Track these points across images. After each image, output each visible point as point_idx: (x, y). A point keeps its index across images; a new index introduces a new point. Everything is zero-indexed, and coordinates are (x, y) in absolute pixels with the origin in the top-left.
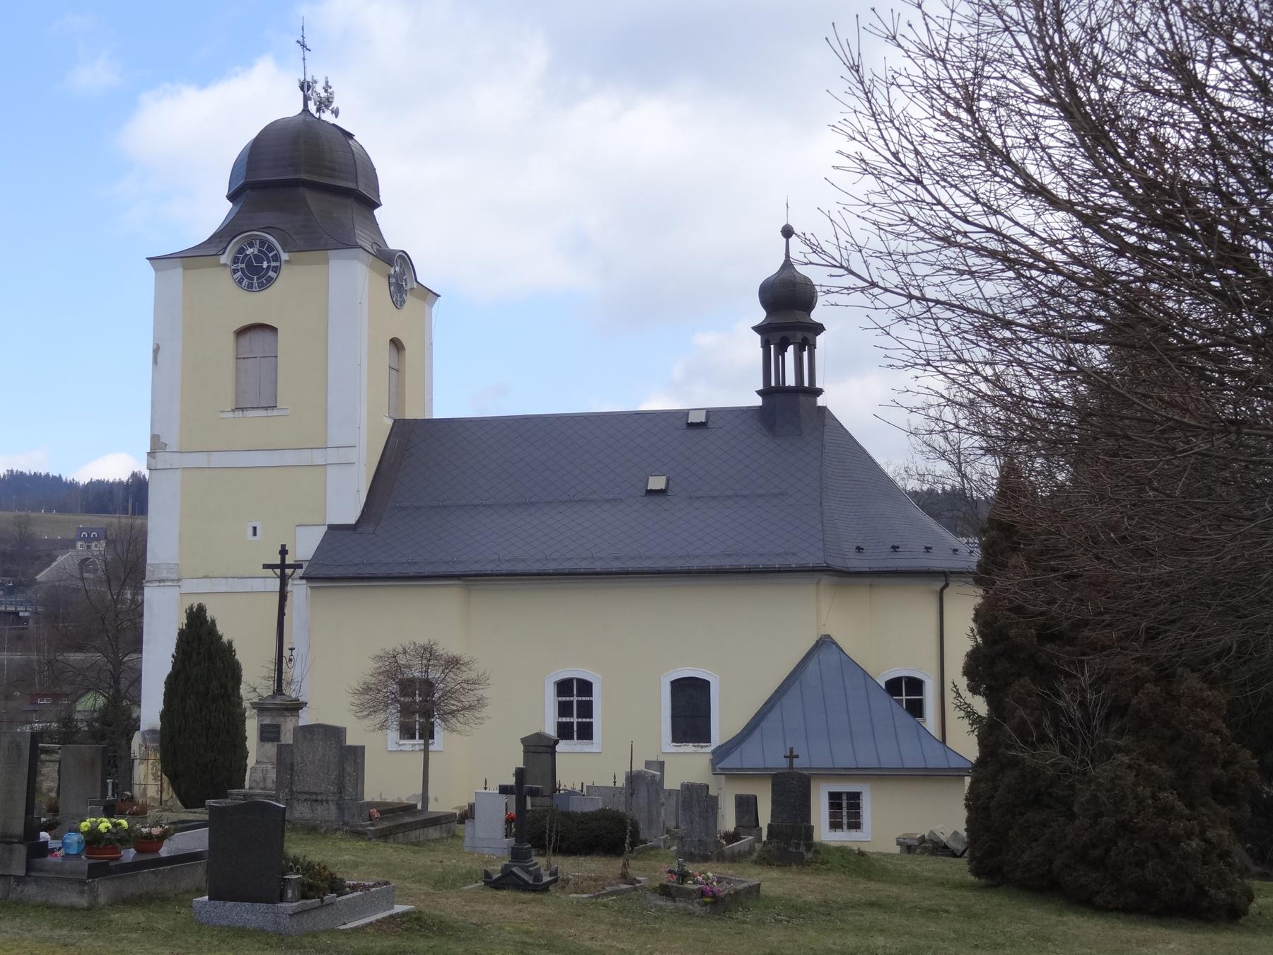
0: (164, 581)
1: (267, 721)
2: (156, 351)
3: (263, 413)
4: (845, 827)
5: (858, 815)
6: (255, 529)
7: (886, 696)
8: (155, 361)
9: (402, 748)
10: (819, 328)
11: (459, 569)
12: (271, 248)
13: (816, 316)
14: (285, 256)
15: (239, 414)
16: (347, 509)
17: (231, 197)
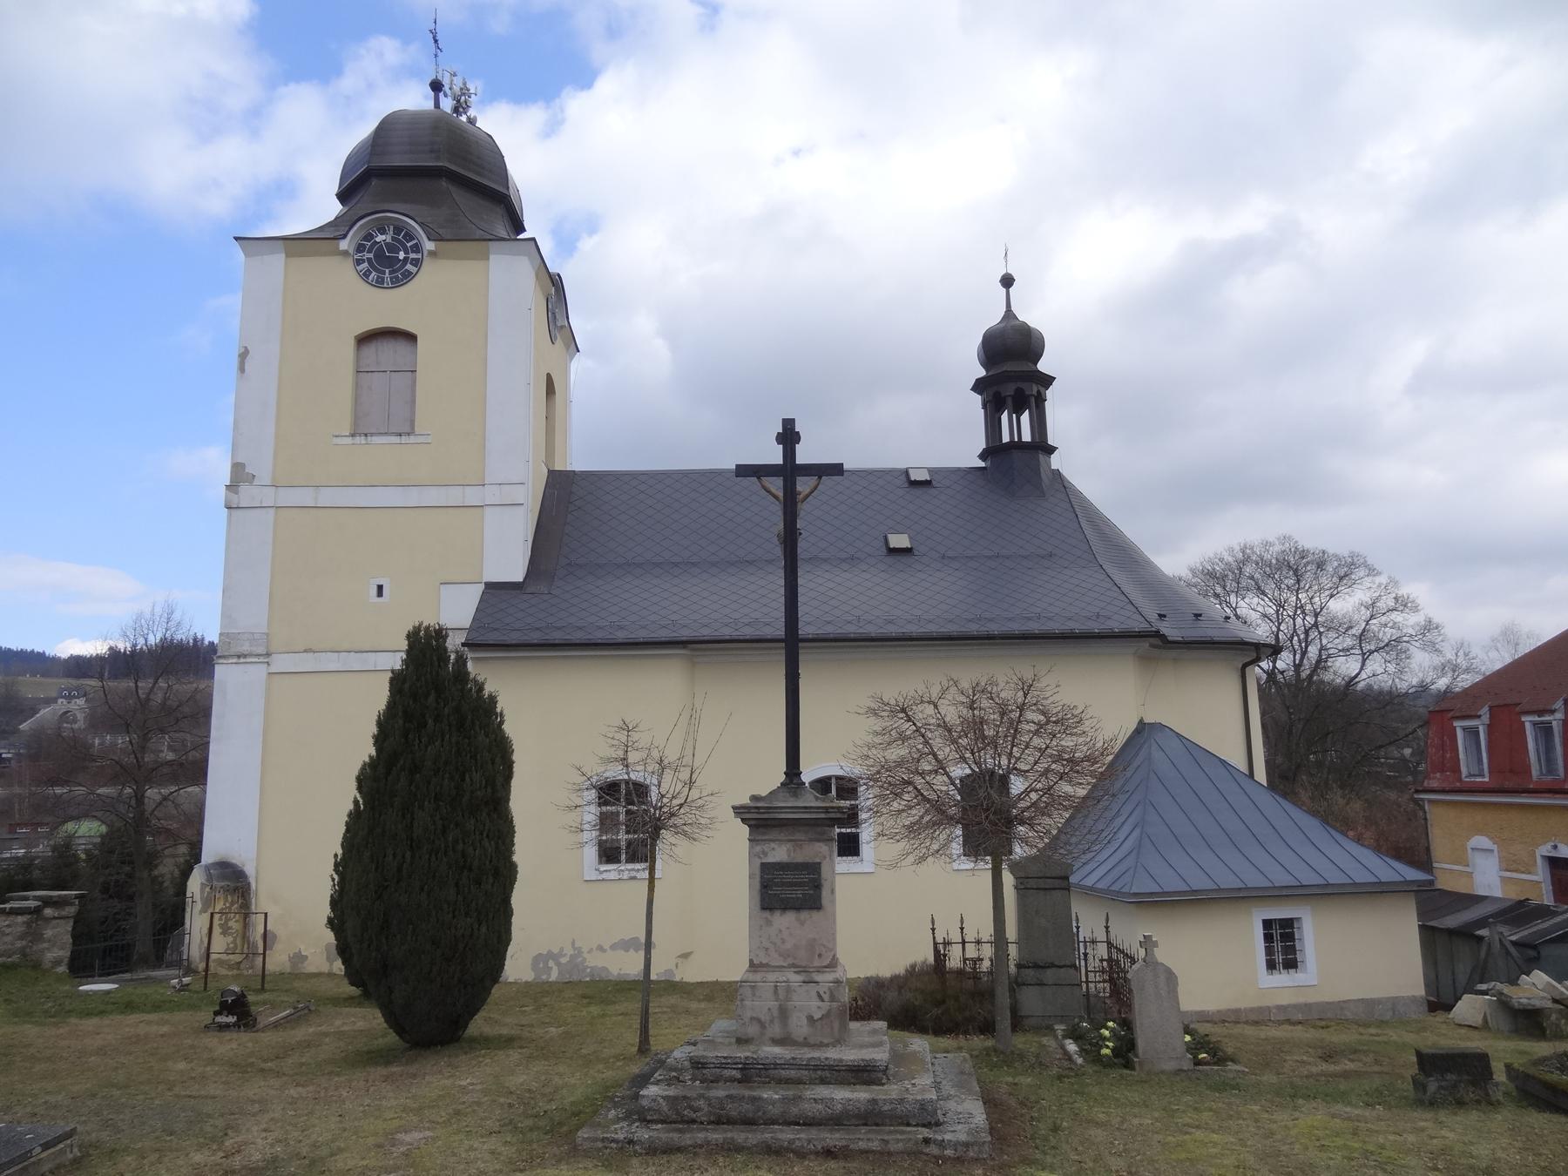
0: (245, 656)
1: (779, 853)
2: (244, 355)
3: (396, 439)
5: (1293, 950)
6: (380, 588)
8: (242, 369)
9: (605, 876)
10: (1048, 381)
11: (685, 634)
12: (410, 236)
13: (1043, 366)
14: (429, 246)
15: (360, 440)
16: (511, 564)
17: (344, 196)
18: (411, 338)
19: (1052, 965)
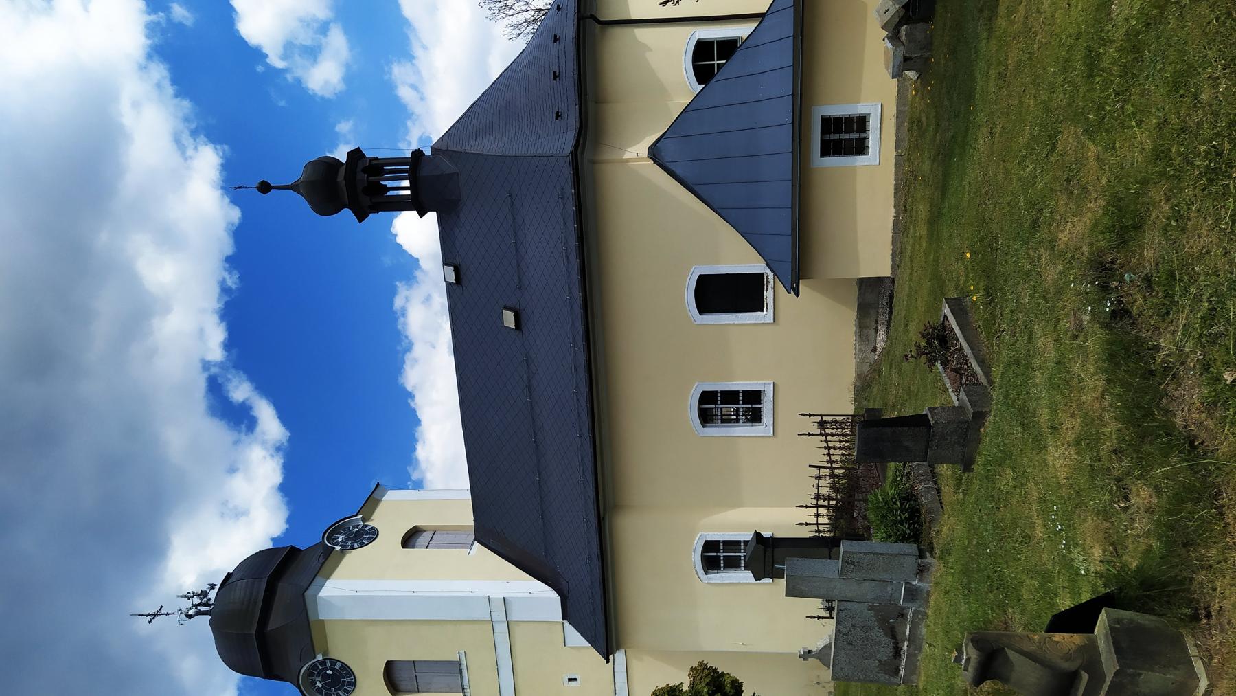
3: (465, 672)
4: (863, 135)
7: (712, 83)
10: (355, 155)
12: (314, 666)
18: (389, 666)
19: (891, 312)
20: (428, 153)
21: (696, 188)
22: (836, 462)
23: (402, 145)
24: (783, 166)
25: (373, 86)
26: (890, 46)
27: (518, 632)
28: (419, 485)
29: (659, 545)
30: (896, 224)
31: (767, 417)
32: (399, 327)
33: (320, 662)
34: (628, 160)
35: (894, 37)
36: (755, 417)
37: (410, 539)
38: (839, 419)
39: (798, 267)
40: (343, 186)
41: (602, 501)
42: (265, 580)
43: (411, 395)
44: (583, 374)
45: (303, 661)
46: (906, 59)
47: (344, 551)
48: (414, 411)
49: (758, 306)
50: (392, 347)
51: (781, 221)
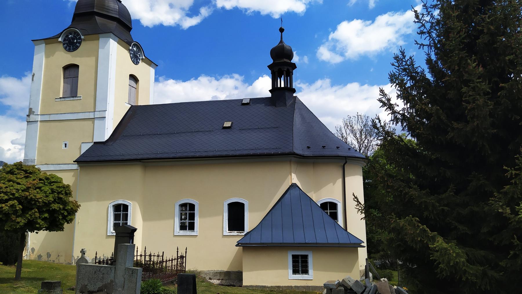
3: (72, 99)
4: (300, 272)
6: (66, 144)
8: (33, 80)
10: (294, 66)
12: (78, 34)
18: (77, 66)
20: (294, 95)
21: (280, 203)
22: (166, 264)
23: (299, 81)
24: (289, 239)
25: (319, 72)
26: (336, 283)
27: (90, 123)
28: (157, 80)
29: (130, 187)
30: (265, 287)
31: (182, 233)
32: (226, 76)
33: (80, 37)
34: (291, 175)
35: (340, 284)
36: (183, 227)
37: (133, 78)
38: (184, 264)
39: (247, 246)
40: (282, 61)
41: (148, 162)
42: (118, 17)
43: (196, 79)
44: (204, 154)
45: (81, 30)
46: (331, 289)
47: (129, 50)
48: (189, 80)
49: (231, 229)
50: (217, 72)
51: (266, 239)
